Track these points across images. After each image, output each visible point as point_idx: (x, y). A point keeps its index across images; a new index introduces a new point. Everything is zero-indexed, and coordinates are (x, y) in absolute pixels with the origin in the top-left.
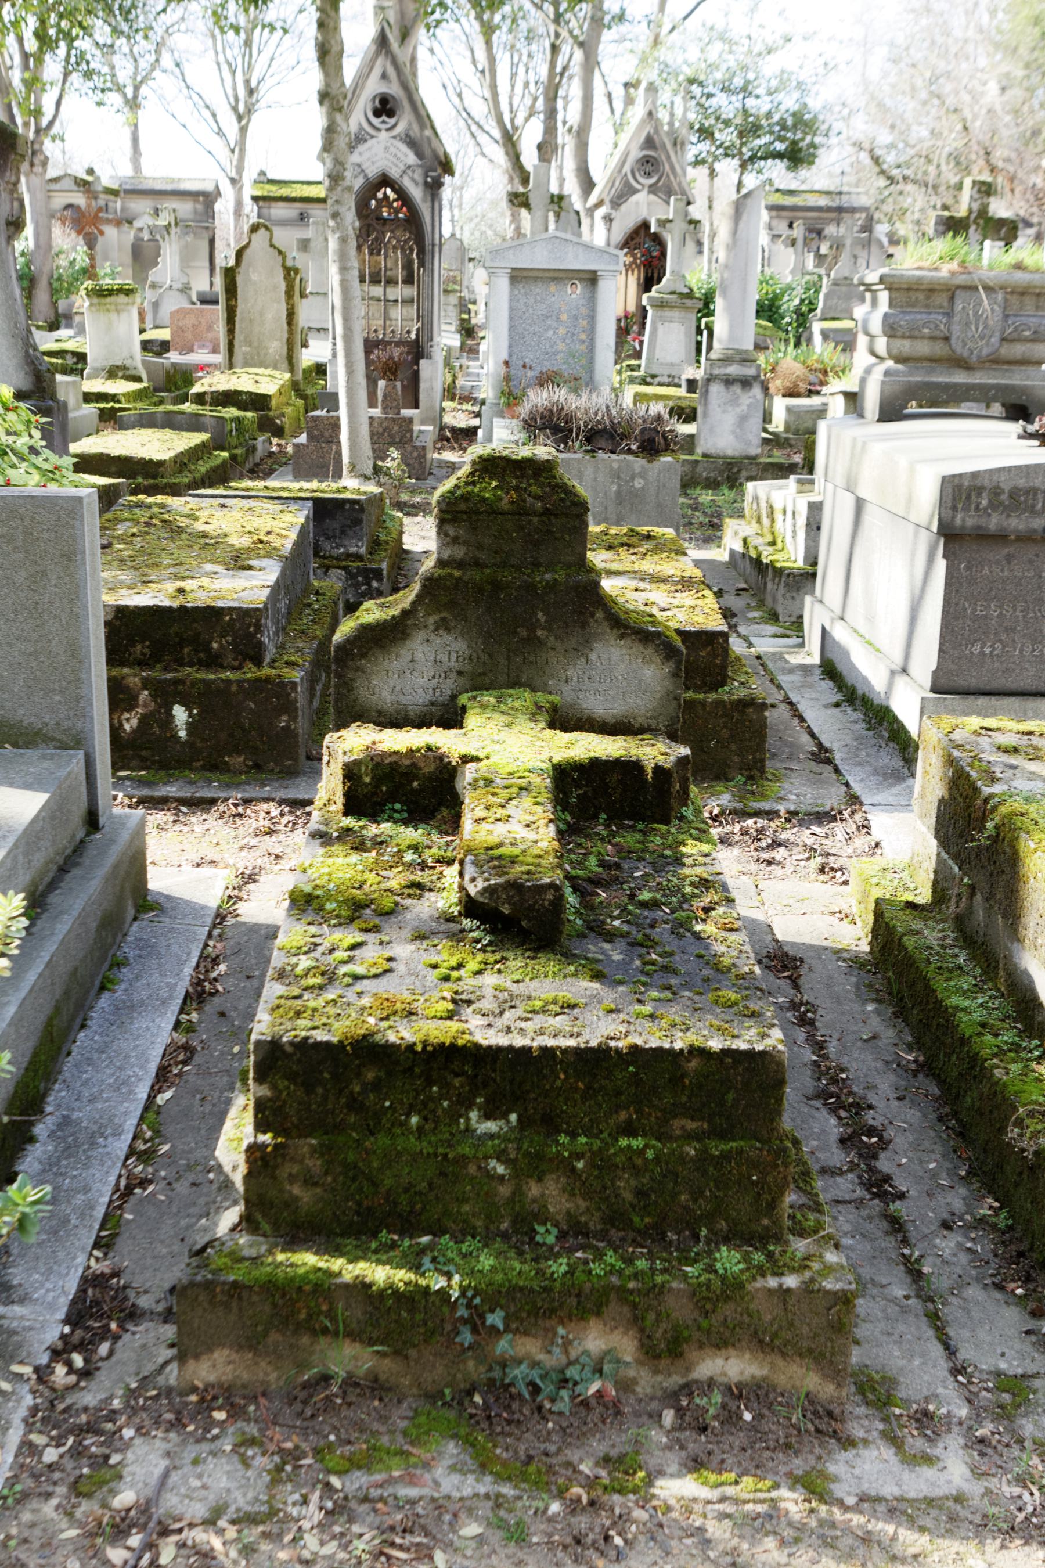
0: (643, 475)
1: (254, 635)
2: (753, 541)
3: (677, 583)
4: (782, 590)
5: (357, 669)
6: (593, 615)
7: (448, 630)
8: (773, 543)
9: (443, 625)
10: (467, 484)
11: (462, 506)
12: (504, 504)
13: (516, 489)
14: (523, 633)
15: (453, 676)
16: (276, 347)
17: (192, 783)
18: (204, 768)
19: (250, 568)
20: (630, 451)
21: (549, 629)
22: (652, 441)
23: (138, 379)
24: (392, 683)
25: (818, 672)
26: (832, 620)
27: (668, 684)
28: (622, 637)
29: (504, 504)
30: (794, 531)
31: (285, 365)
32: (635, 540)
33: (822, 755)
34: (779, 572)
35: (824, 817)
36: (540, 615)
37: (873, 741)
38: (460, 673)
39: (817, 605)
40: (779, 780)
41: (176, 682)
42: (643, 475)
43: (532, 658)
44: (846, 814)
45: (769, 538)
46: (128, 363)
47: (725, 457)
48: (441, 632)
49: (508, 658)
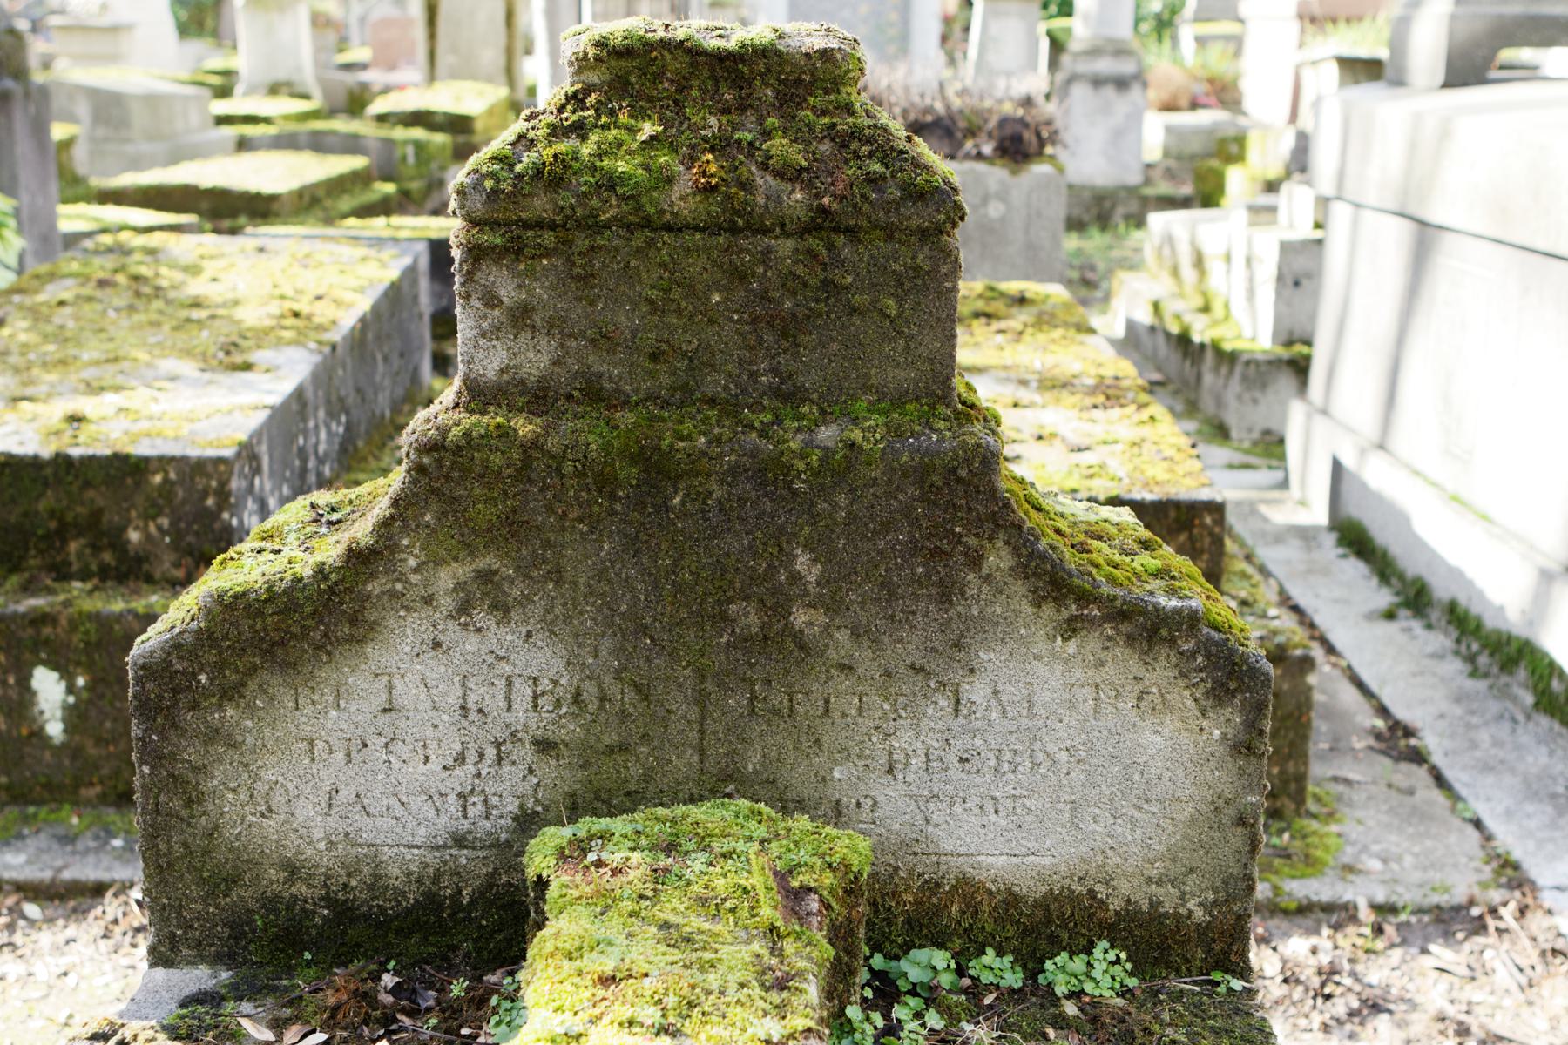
0: (1003, 196)
1: (214, 515)
2: (1169, 308)
3: (1093, 391)
4: (1235, 385)
5: (213, 736)
6: (975, 561)
7: (502, 610)
8: (1206, 309)
9: (484, 597)
10: (557, 132)
11: (541, 205)
12: (681, 197)
13: (720, 146)
14: (749, 618)
15: (524, 753)
16: (491, 56)
17: (68, 839)
18: (103, 799)
19: (247, 367)
20: (979, 156)
21: (833, 606)
22: (1017, 139)
23: (306, 96)
24: (326, 778)
25: (1330, 539)
26: (1363, 452)
27: (1222, 777)
28: (1070, 629)
29: (681, 197)
30: (1251, 293)
31: (502, 78)
32: (998, 306)
33: (1398, 741)
34: (1227, 359)
35: (1453, 920)
36: (802, 560)
37: (1494, 707)
38: (544, 746)
39: (1320, 423)
40: (1331, 816)
41: (40, 619)
42: (1003, 196)
43: (778, 699)
44: (1508, 913)
45: (1198, 302)
46: (295, 77)
47: (1093, 189)
48: (480, 618)
49: (701, 698)
